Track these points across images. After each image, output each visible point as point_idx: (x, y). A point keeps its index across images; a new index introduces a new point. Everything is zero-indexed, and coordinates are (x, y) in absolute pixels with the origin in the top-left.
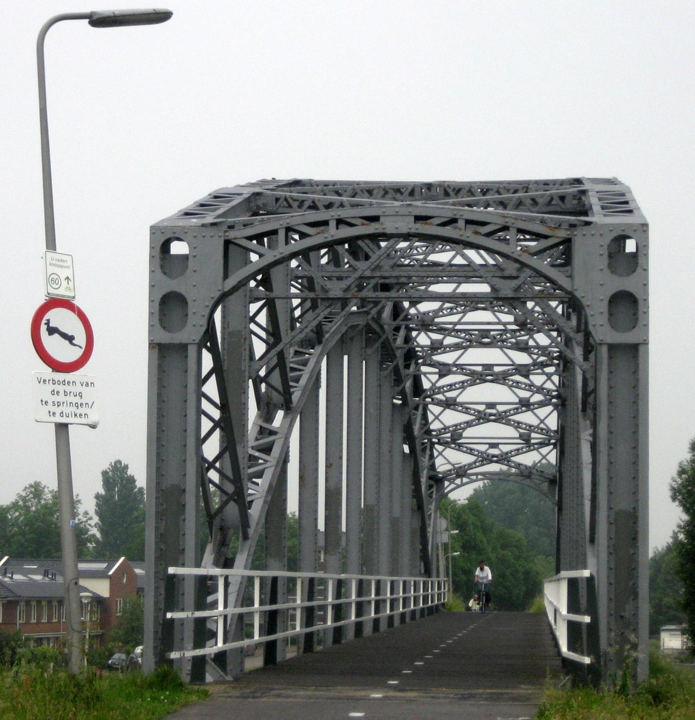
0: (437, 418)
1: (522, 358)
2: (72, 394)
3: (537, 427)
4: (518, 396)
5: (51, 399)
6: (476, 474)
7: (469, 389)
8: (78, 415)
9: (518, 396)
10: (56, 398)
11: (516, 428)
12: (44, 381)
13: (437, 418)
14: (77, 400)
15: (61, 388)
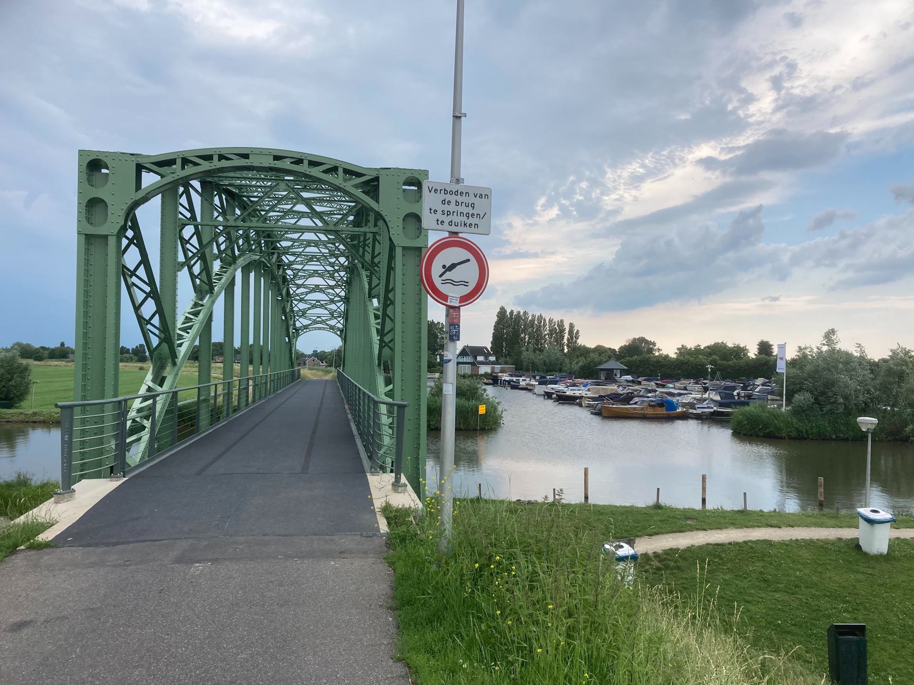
0: (296, 305)
1: (332, 283)
2: (463, 204)
5: (440, 207)
7: (309, 295)
8: (468, 225)
10: (446, 208)
12: (436, 191)
13: (296, 305)
14: (470, 210)
15: (453, 198)
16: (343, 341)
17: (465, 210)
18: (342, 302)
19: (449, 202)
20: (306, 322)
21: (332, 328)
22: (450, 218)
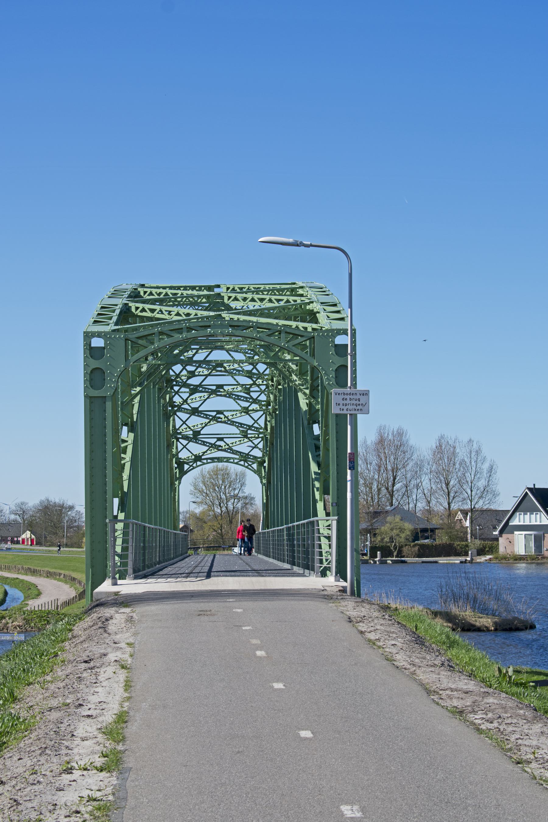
3: (252, 426)
4: (241, 406)
5: (342, 402)
6: (207, 459)
9: (241, 406)
10: (345, 402)
11: (237, 427)
12: (339, 394)
14: (358, 402)
15: (348, 397)
16: (264, 481)
17: (355, 402)
18: (262, 413)
19: (346, 399)
20: (197, 449)
21: (245, 457)
22: (347, 407)
